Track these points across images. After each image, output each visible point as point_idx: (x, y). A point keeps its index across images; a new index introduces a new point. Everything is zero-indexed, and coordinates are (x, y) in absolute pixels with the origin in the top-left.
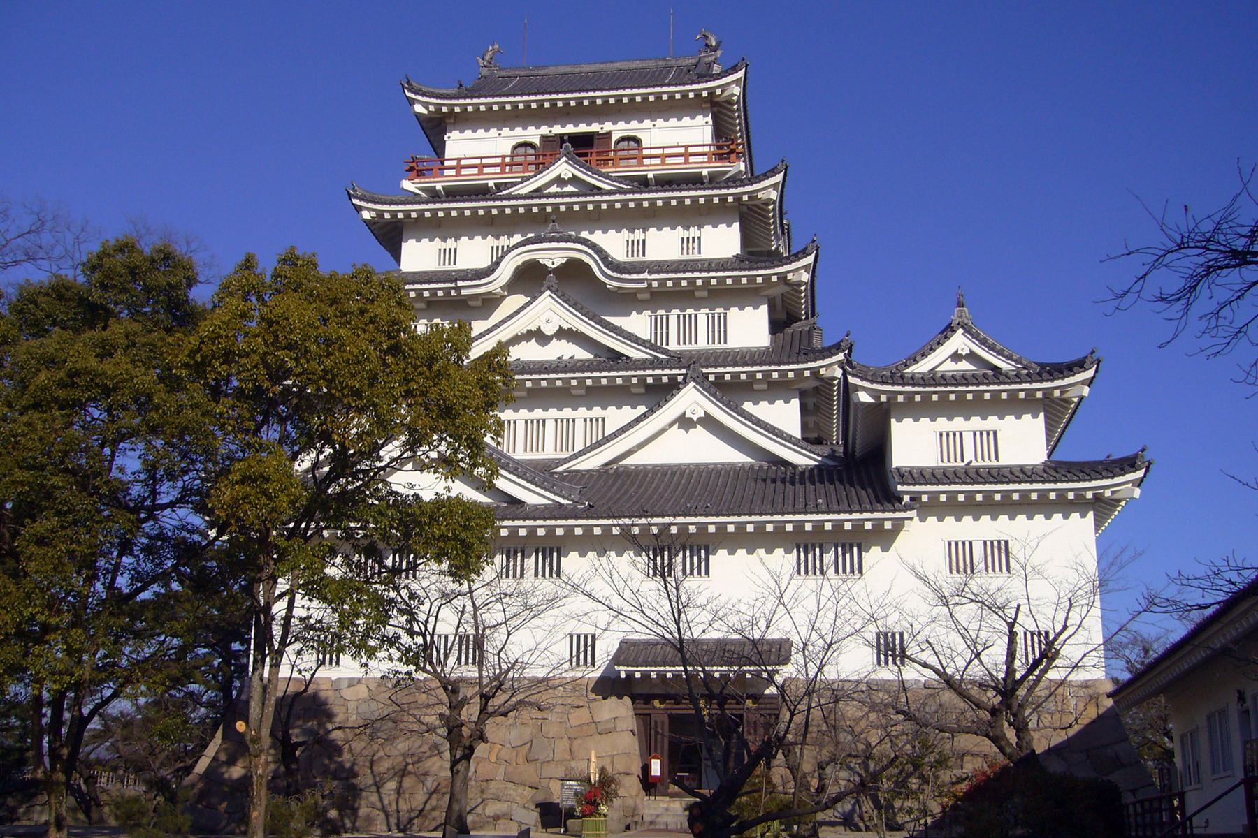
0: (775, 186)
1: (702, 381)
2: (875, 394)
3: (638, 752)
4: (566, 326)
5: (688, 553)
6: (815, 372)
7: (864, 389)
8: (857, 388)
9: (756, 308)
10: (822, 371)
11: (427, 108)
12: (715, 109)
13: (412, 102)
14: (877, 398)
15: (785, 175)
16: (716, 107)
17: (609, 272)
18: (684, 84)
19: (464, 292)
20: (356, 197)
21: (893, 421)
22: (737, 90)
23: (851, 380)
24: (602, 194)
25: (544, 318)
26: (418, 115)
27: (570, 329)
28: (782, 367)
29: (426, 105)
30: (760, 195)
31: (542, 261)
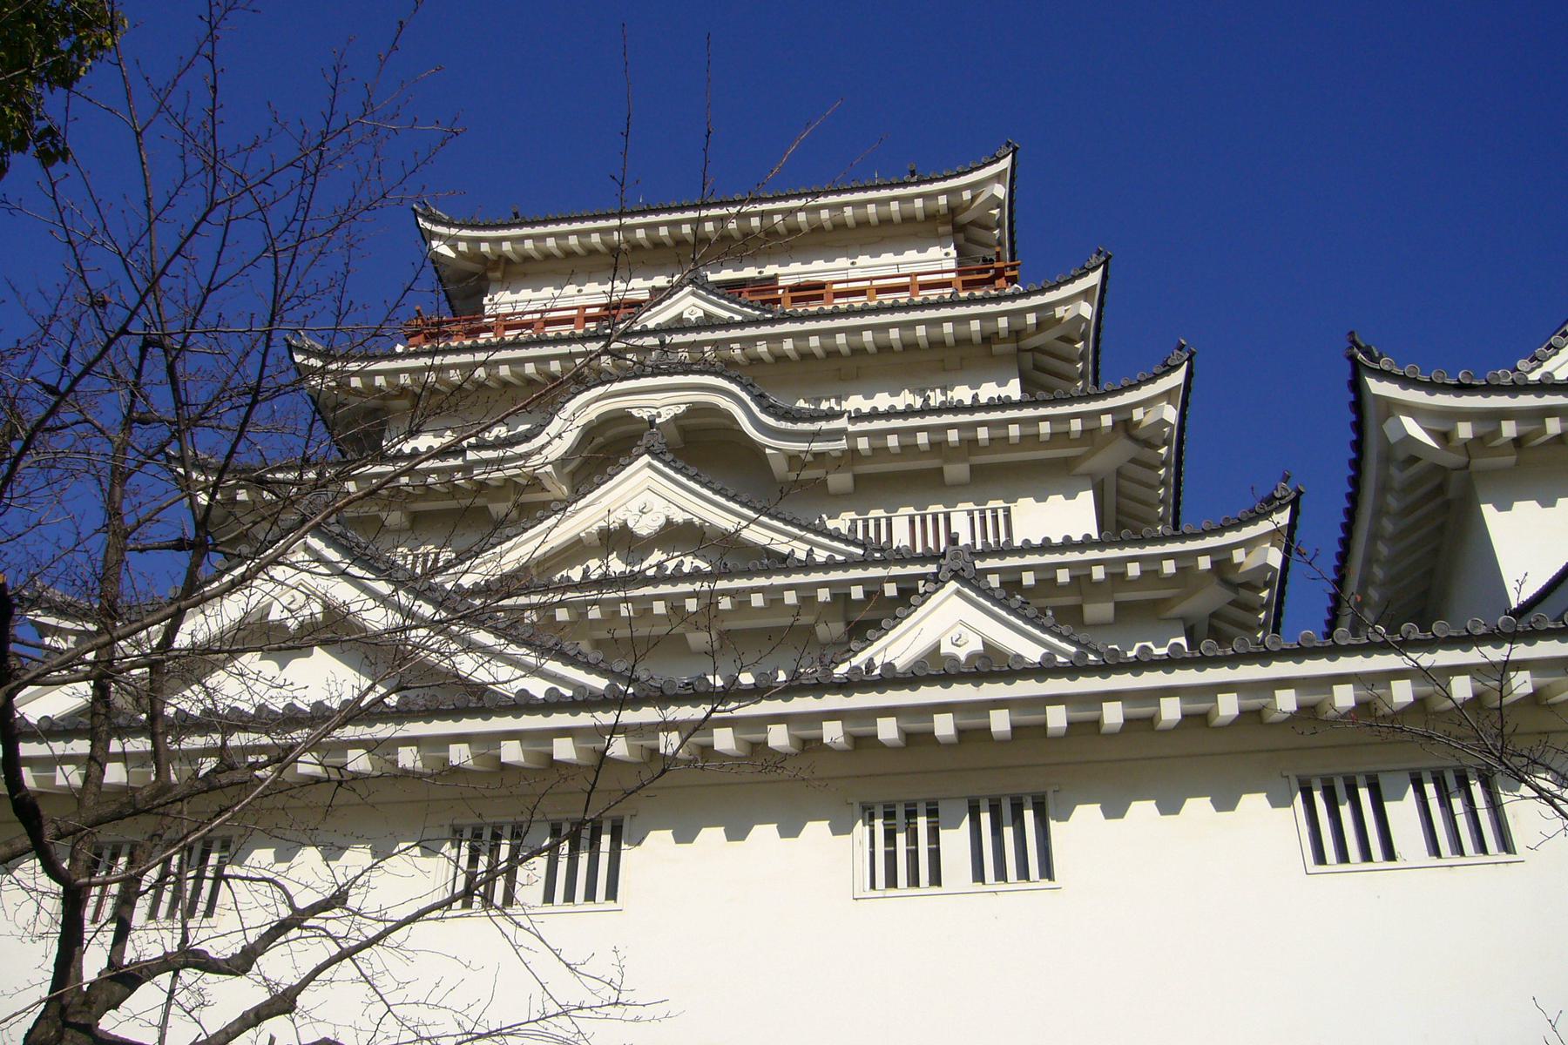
0: (1086, 294)
1: (972, 580)
3: (113, 1032)
4: (679, 517)
5: (985, 818)
8: (1391, 408)
9: (1071, 495)
10: (1238, 556)
11: (454, 247)
12: (961, 236)
13: (428, 236)
14: (1444, 437)
17: (770, 421)
18: (905, 184)
19: (478, 474)
20: (301, 350)
21: (1488, 510)
23: (1376, 387)
25: (635, 506)
26: (438, 259)
27: (688, 524)
28: (1149, 550)
29: (452, 241)
30: (1059, 312)
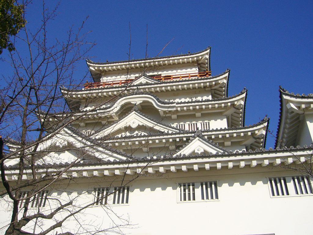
0: (225, 78)
1: (202, 137)
2: (299, 105)
3: (24, 231)
4: (141, 124)
6: (253, 133)
7: (292, 102)
8: (288, 101)
9: (222, 120)
11: (94, 68)
15: (229, 74)
16: (198, 63)
20: (63, 89)
22: (207, 57)
24: (163, 135)
26: (91, 71)
27: (143, 126)
29: (94, 67)
30: (220, 82)
31: (132, 102)
